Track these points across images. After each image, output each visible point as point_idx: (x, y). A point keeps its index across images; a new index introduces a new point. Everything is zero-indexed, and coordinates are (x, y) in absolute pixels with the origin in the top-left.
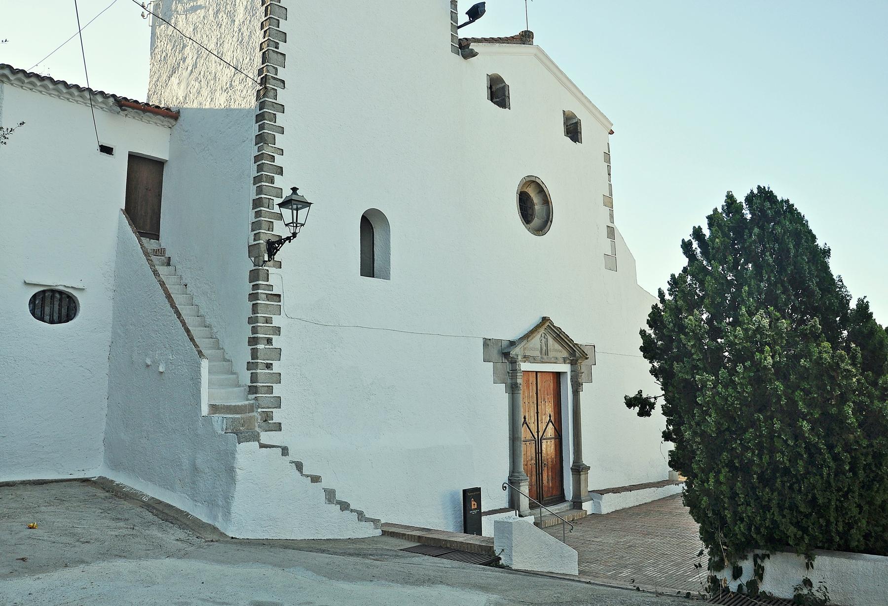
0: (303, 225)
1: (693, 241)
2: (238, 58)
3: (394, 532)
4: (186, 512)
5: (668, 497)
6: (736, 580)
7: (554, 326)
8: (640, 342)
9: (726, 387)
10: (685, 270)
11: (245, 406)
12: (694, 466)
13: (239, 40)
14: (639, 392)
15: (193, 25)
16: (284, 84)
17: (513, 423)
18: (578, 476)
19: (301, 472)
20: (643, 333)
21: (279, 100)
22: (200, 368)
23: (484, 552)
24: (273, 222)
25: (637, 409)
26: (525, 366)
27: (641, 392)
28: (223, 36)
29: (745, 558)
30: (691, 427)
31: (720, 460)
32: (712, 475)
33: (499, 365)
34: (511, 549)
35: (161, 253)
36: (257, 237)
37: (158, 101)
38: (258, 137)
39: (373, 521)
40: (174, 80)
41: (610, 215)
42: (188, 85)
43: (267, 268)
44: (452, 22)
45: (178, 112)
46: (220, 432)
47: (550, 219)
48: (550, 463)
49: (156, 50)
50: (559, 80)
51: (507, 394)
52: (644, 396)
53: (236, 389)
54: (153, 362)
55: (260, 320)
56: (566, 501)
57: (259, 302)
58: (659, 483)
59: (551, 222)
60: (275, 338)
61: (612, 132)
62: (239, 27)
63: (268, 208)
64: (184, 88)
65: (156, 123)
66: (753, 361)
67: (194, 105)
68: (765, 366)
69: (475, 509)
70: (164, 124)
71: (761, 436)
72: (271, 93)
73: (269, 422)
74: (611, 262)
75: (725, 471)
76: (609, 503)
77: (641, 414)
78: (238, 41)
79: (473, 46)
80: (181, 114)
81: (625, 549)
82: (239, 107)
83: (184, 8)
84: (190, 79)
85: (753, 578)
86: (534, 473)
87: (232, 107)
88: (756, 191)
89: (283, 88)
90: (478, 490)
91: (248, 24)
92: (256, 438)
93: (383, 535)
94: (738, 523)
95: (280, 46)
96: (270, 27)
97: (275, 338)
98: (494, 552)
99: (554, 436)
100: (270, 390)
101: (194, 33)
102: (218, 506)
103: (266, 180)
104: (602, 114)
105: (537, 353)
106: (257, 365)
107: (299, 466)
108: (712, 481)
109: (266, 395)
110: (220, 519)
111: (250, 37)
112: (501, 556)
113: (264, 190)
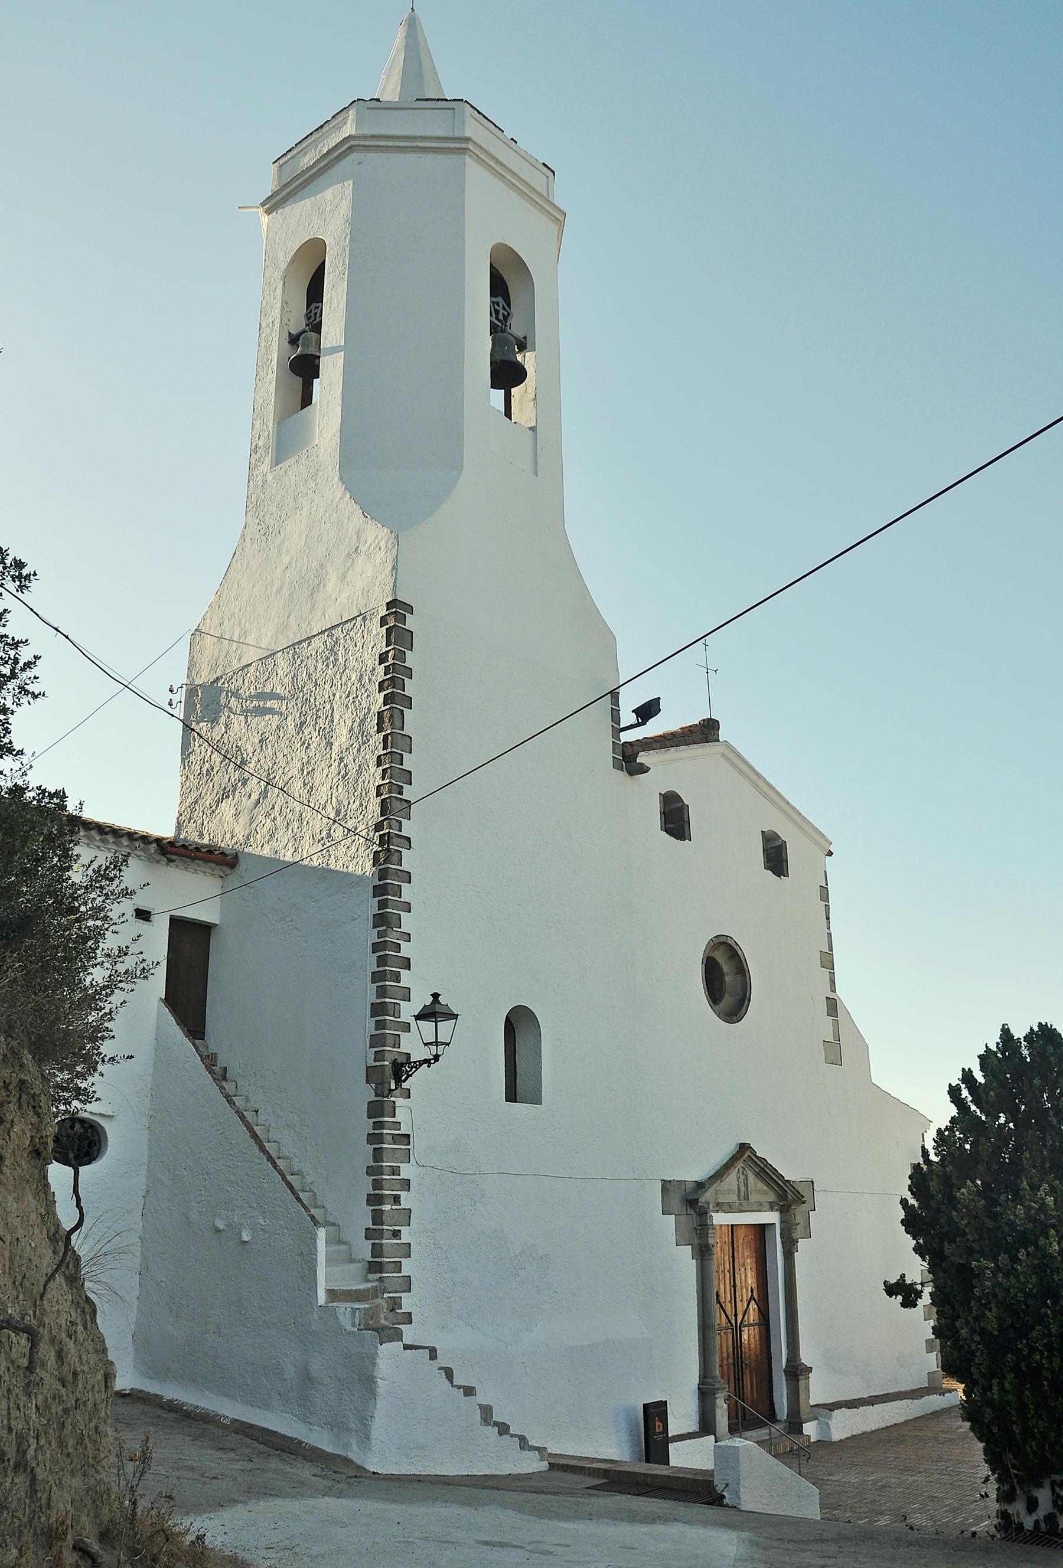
0: (448, 1044)
1: (961, 1085)
2: (339, 799)
3: (567, 1466)
4: (296, 1439)
5: (928, 1414)
6: (1031, 1514)
7: (757, 1157)
8: (902, 1215)
9: (1007, 1275)
10: (953, 1120)
11: (368, 1290)
12: (974, 1370)
13: (340, 772)
14: (901, 1276)
15: (260, 734)
16: (410, 842)
17: (703, 1303)
18: (795, 1382)
19: (452, 1383)
20: (904, 1202)
21: (405, 867)
22: (315, 1240)
23: (700, 1489)
24: (399, 1035)
25: (900, 1298)
26: (719, 1219)
27: (904, 1277)
28: (313, 762)
29: (1040, 1485)
30: (968, 1323)
31: (1005, 1364)
32: (995, 1382)
33: (683, 1218)
34: (738, 1484)
35: (212, 1061)
36: (379, 1056)
37: (197, 833)
38: (377, 917)
39: (538, 1449)
40: (227, 808)
41: (830, 979)
42: (252, 820)
43: (393, 1099)
44: (613, 724)
45: (236, 856)
46: (349, 1328)
47: (748, 996)
48: (754, 1363)
49: (192, 757)
50: (756, 786)
51: (695, 1260)
52: (908, 1281)
53: (352, 1266)
54: (229, 1225)
55: (387, 1170)
56: (778, 1421)
57: (384, 1146)
58: (914, 1391)
59: (749, 1000)
60: (403, 1194)
61: (830, 854)
62: (341, 755)
63: (393, 1016)
64: (246, 824)
65: (204, 872)
66: (1037, 1246)
67: (265, 852)
68: (1051, 1253)
69: (660, 1433)
70: (215, 872)
71: (1050, 1334)
72: (395, 858)
73: (398, 1311)
74: (834, 1052)
75: (1010, 1376)
76: (842, 1425)
77: (904, 1305)
78: (339, 773)
79: (642, 758)
80: (241, 860)
81: (876, 1490)
82: (345, 870)
83: (242, 706)
84: (255, 812)
85: (1052, 1511)
86: (732, 1378)
87: (332, 867)
88: (1036, 1029)
89: (408, 847)
90: (663, 1404)
91: (355, 754)
92: (398, 1336)
93: (550, 1469)
94: (1029, 1440)
95: (405, 791)
96: (392, 765)
97: (403, 1194)
98: (714, 1488)
99: (757, 1322)
100: (398, 1267)
101: (262, 746)
102: (349, 1430)
103: (391, 978)
104: (816, 829)
105: (733, 1198)
106: (383, 1233)
107: (449, 1374)
108: (995, 1389)
109: (393, 1275)
110: (355, 1448)
111: (359, 772)
112: (725, 1493)
113: (388, 992)
